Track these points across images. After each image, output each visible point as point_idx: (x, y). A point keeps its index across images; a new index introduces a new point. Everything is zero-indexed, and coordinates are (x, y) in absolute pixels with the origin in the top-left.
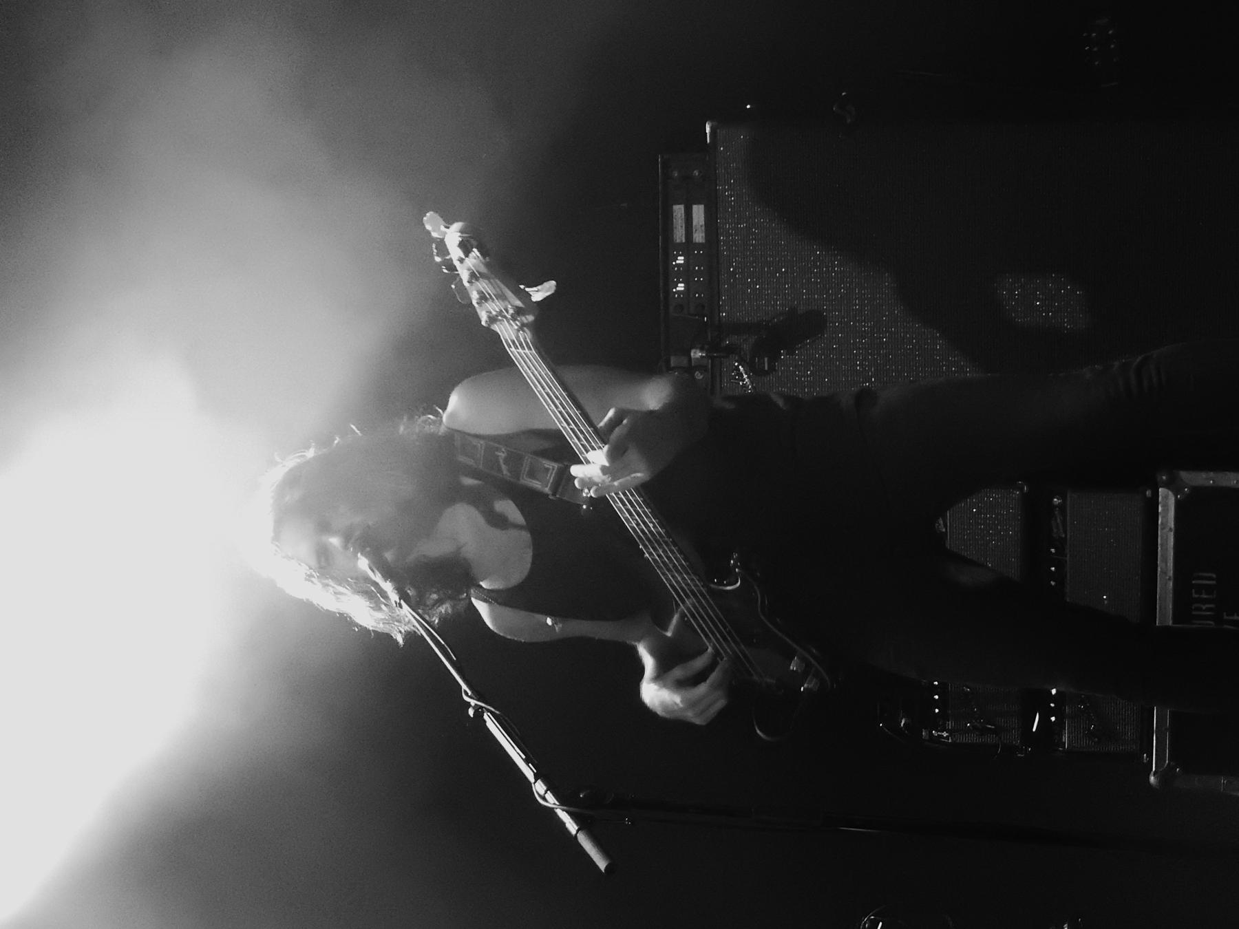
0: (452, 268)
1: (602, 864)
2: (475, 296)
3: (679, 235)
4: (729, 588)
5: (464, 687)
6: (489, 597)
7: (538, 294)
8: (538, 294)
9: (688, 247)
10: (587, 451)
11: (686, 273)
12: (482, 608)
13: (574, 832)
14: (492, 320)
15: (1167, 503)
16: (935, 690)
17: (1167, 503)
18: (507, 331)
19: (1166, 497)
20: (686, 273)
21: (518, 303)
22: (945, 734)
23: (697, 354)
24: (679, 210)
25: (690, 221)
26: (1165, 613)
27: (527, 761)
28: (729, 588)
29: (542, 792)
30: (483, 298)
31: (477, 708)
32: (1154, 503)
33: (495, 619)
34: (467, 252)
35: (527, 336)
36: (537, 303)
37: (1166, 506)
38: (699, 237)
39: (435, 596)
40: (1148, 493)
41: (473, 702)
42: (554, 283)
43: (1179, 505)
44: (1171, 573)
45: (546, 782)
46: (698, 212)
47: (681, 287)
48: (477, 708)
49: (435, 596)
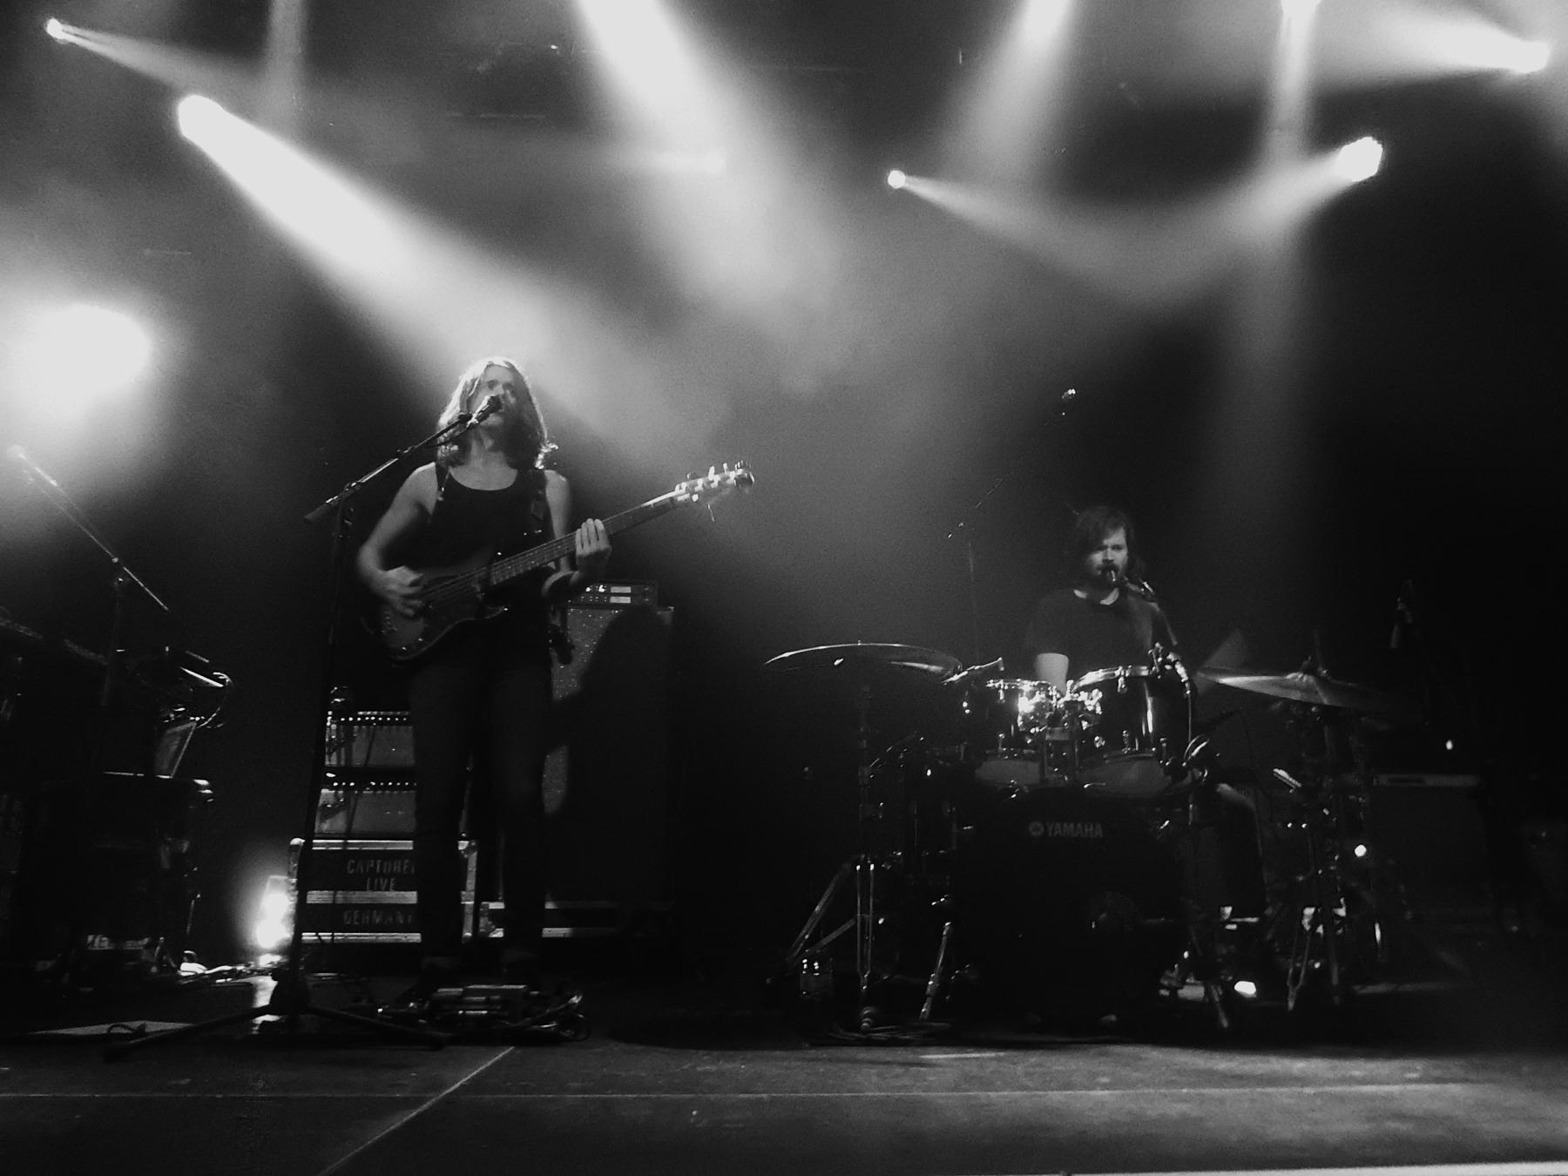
3: (615, 589)
9: (608, 594)
11: (595, 592)
24: (628, 590)
38: (614, 600)
46: (627, 600)
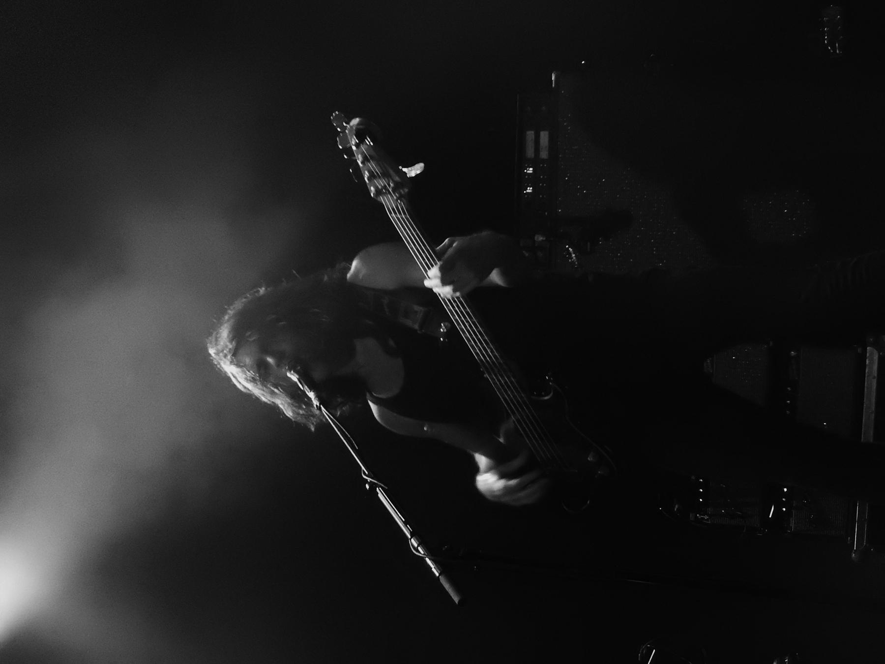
0: (349, 151)
1: (456, 599)
2: (366, 175)
3: (530, 153)
4: (546, 398)
5: (363, 468)
6: (377, 402)
7: (413, 171)
8: (413, 171)
10: (429, 269)
11: (532, 180)
12: (374, 407)
13: (437, 575)
14: (379, 192)
15: (873, 358)
16: (701, 485)
17: (873, 358)
18: (389, 202)
19: (872, 354)
20: (532, 180)
21: (397, 179)
22: (706, 517)
23: (540, 238)
24: (530, 135)
25: (539, 142)
26: (868, 434)
27: (405, 523)
28: (546, 398)
29: (416, 545)
30: (372, 176)
31: (371, 484)
32: (863, 357)
33: (380, 416)
34: (361, 139)
35: (401, 204)
36: (412, 178)
37: (872, 360)
38: (544, 155)
39: (339, 400)
40: (859, 350)
41: (369, 479)
42: (422, 165)
43: (880, 358)
44: (873, 408)
45: (417, 540)
46: (544, 136)
47: (530, 190)
48: (371, 484)
49: (339, 400)
